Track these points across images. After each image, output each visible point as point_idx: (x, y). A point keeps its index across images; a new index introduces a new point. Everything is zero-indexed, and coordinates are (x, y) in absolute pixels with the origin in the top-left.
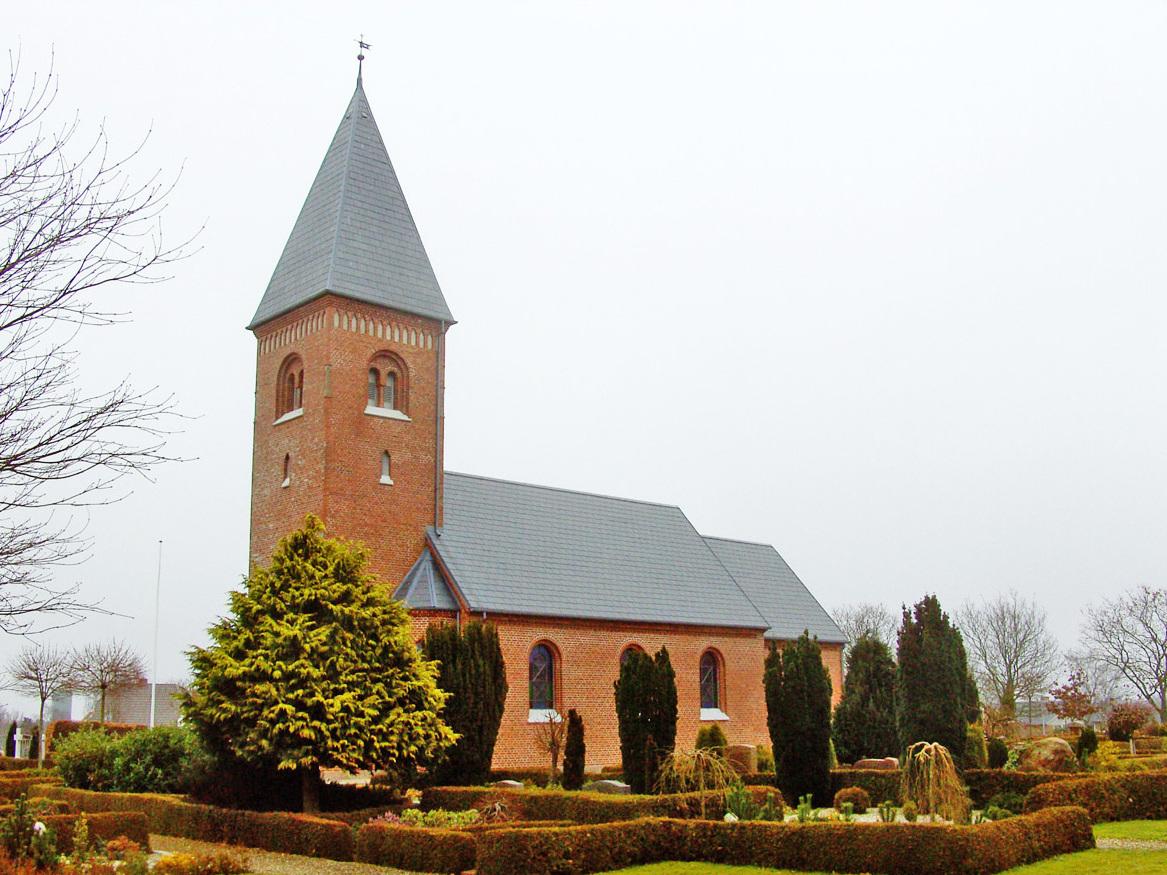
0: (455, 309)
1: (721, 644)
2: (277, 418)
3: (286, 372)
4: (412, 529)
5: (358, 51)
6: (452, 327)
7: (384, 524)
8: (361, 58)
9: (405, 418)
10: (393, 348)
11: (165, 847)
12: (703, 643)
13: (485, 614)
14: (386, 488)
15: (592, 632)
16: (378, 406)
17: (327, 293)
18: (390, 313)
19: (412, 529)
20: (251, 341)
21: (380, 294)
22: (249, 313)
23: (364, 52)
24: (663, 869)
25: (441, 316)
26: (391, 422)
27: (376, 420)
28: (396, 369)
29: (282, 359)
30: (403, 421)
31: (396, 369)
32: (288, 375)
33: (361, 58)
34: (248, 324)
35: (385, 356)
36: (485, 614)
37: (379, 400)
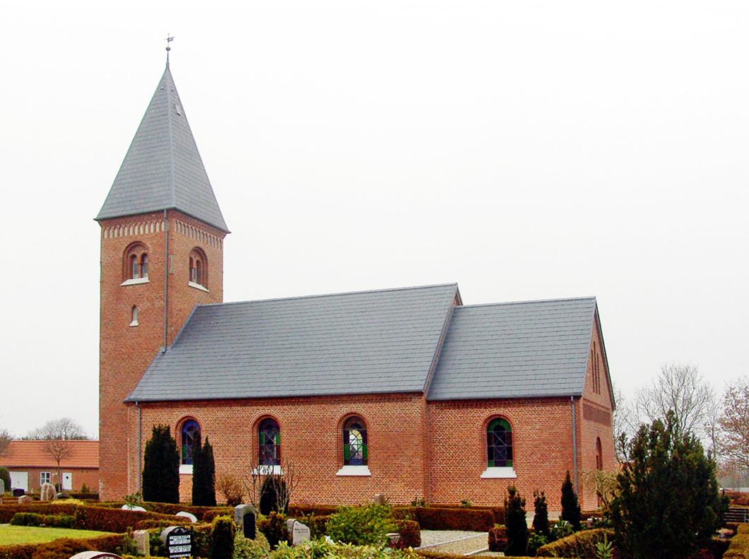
0: (230, 221)
1: (199, 414)
2: (123, 281)
3: (129, 252)
4: (150, 350)
5: (166, 44)
6: (228, 235)
7: (133, 351)
8: (168, 49)
9: (206, 290)
10: (138, 239)
11: (494, 512)
12: (486, 413)
13: (572, 398)
14: (135, 328)
15: (227, 408)
16: (142, 277)
17: (175, 209)
18: (193, 220)
19: (150, 350)
20: (97, 228)
21: (128, 208)
22: (96, 206)
23: (171, 45)
24: (34, 535)
25: (224, 228)
26: (137, 286)
27: (128, 288)
28: (200, 260)
29: (202, 248)
30: (202, 290)
31: (200, 260)
32: (130, 255)
33: (168, 49)
34: (95, 218)
35: (198, 252)
36: (572, 398)
37: (142, 273)
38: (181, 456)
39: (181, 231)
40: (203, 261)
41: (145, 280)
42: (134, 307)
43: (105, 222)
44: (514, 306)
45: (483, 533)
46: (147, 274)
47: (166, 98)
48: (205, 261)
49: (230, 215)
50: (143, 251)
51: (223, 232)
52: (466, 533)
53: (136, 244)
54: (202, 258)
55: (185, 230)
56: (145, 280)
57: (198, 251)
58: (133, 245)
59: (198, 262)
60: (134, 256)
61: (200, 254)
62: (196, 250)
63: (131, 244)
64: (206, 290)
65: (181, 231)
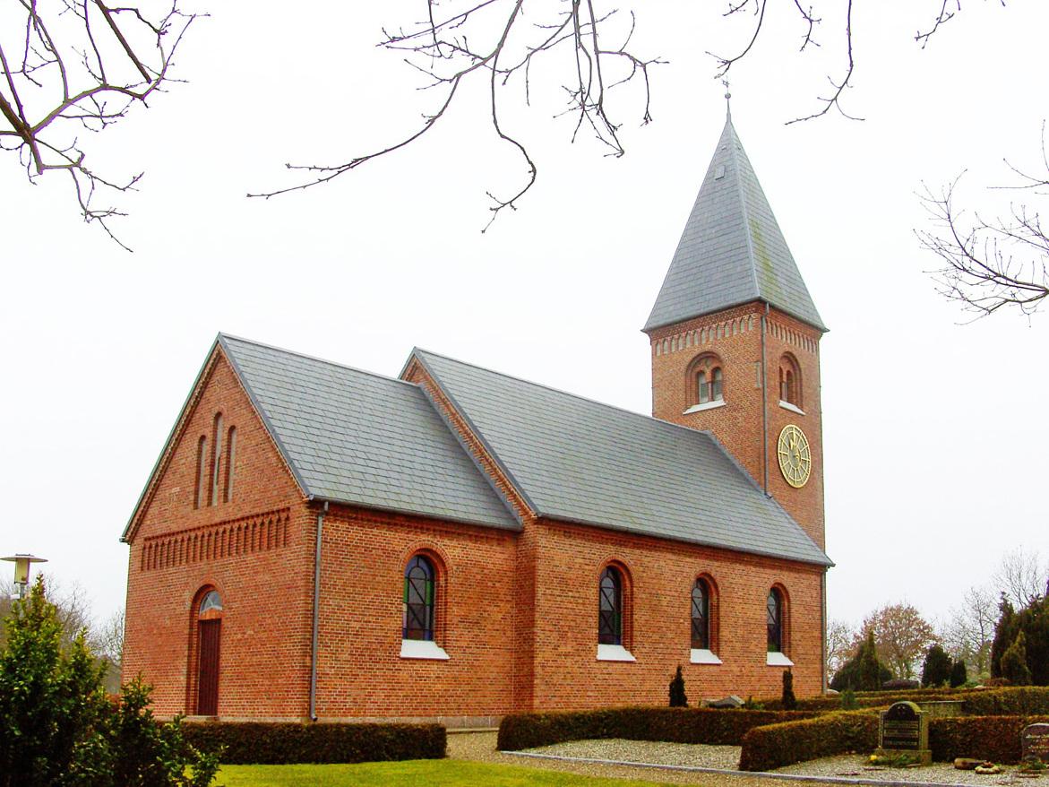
3: (694, 367)
20: (646, 338)
22: (643, 317)
31: (792, 371)
34: (642, 328)
35: (790, 361)
38: (875, 699)
39: (777, 336)
40: (795, 370)
41: (719, 402)
42: (219, 415)
43: (658, 332)
44: (568, 397)
45: (228, 719)
46: (720, 396)
47: (735, 174)
48: (798, 372)
49: (825, 307)
50: (715, 365)
51: (814, 331)
52: (405, 763)
53: (709, 356)
54: (793, 367)
55: (772, 328)
56: (719, 402)
57: (789, 357)
58: (791, 358)
59: (789, 373)
60: (701, 373)
61: (792, 364)
62: (785, 356)
63: (794, 357)
64: (801, 412)
65: (777, 336)
